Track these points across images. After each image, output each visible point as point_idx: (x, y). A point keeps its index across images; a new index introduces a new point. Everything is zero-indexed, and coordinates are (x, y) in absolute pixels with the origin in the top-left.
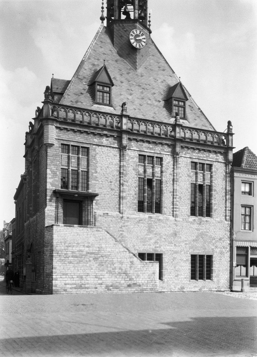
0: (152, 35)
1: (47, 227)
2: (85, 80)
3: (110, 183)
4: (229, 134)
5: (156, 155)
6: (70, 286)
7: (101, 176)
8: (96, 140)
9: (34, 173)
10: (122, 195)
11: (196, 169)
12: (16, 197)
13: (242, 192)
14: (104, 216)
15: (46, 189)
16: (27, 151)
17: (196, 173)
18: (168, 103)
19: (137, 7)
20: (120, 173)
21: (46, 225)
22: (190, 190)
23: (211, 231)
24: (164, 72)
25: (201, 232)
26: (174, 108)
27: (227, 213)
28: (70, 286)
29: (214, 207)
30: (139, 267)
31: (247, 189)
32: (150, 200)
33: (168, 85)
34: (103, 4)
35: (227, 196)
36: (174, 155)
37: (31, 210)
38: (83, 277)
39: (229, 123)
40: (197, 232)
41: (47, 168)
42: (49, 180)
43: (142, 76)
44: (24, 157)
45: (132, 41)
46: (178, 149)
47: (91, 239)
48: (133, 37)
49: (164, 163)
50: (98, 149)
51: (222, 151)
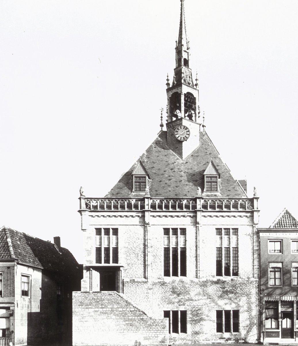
3: (137, 255)
7: (129, 250)
8: (124, 221)
14: (131, 282)
23: (236, 288)
25: (226, 290)
27: (255, 271)
30: (149, 323)
32: (176, 262)
35: (255, 256)
40: (222, 290)
47: (104, 301)
51: (248, 215)
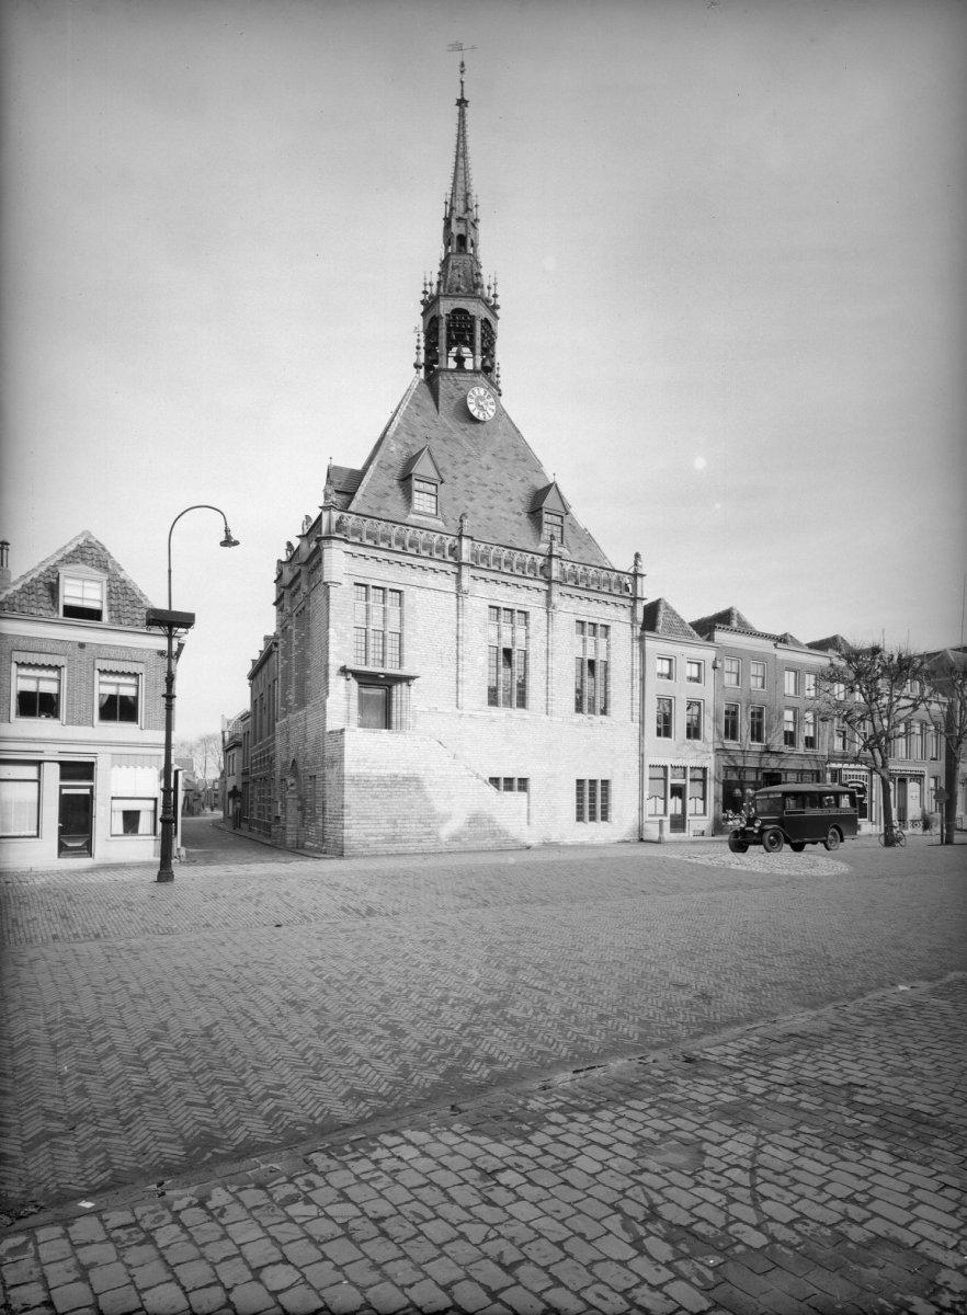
0: (502, 400)
1: (331, 732)
2: (391, 471)
5: (518, 608)
6: (374, 838)
8: (416, 577)
9: (298, 634)
10: (460, 676)
11: (583, 632)
12: (253, 676)
13: (659, 674)
15: (327, 665)
16: (282, 595)
17: (584, 641)
18: (535, 512)
19: (478, 350)
20: (457, 637)
21: (328, 730)
22: (574, 669)
24: (524, 464)
26: (545, 526)
28: (374, 838)
29: (614, 698)
31: (666, 671)
33: (533, 486)
34: (418, 340)
37: (290, 701)
38: (399, 821)
39: (637, 556)
41: (328, 627)
42: (332, 648)
43: (489, 469)
44: (275, 604)
45: (471, 407)
46: (555, 599)
48: (473, 401)
49: (531, 621)
50: (420, 594)
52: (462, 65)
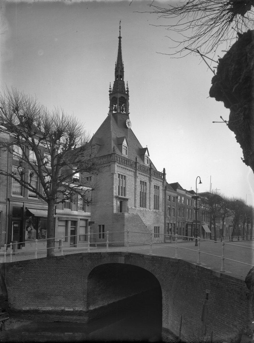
4: (164, 174)
36: (150, 181)
52: (120, 27)
